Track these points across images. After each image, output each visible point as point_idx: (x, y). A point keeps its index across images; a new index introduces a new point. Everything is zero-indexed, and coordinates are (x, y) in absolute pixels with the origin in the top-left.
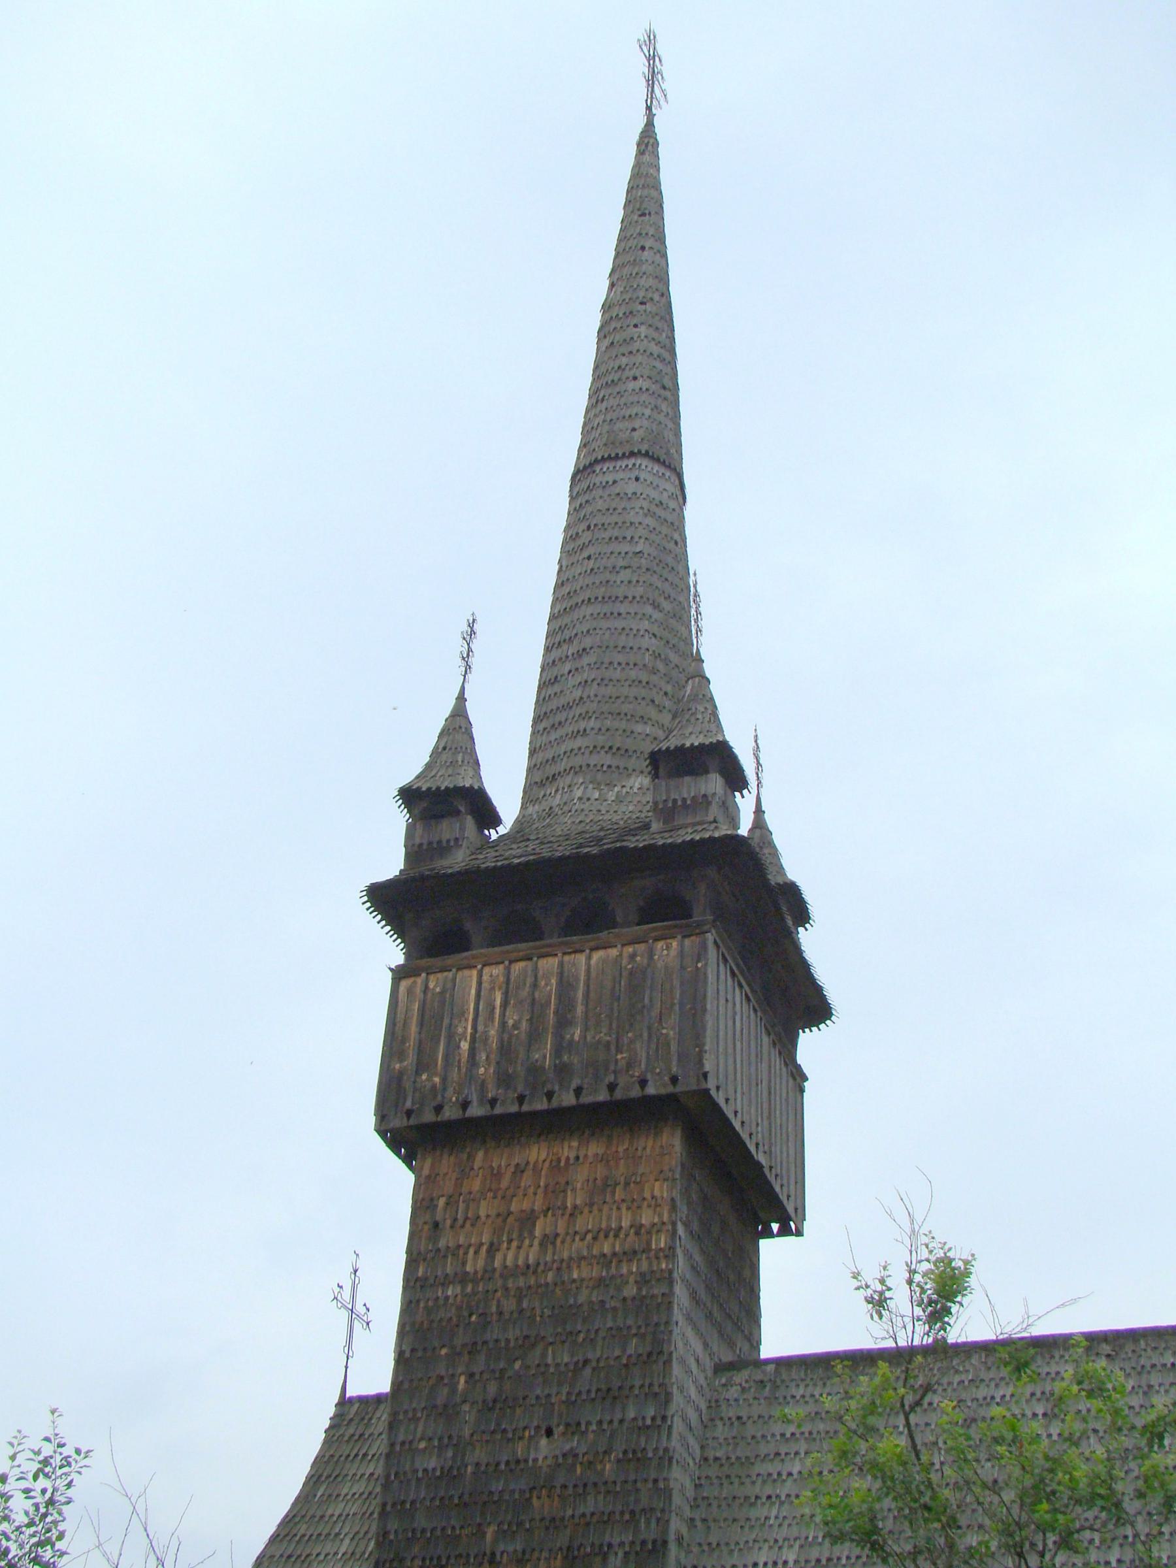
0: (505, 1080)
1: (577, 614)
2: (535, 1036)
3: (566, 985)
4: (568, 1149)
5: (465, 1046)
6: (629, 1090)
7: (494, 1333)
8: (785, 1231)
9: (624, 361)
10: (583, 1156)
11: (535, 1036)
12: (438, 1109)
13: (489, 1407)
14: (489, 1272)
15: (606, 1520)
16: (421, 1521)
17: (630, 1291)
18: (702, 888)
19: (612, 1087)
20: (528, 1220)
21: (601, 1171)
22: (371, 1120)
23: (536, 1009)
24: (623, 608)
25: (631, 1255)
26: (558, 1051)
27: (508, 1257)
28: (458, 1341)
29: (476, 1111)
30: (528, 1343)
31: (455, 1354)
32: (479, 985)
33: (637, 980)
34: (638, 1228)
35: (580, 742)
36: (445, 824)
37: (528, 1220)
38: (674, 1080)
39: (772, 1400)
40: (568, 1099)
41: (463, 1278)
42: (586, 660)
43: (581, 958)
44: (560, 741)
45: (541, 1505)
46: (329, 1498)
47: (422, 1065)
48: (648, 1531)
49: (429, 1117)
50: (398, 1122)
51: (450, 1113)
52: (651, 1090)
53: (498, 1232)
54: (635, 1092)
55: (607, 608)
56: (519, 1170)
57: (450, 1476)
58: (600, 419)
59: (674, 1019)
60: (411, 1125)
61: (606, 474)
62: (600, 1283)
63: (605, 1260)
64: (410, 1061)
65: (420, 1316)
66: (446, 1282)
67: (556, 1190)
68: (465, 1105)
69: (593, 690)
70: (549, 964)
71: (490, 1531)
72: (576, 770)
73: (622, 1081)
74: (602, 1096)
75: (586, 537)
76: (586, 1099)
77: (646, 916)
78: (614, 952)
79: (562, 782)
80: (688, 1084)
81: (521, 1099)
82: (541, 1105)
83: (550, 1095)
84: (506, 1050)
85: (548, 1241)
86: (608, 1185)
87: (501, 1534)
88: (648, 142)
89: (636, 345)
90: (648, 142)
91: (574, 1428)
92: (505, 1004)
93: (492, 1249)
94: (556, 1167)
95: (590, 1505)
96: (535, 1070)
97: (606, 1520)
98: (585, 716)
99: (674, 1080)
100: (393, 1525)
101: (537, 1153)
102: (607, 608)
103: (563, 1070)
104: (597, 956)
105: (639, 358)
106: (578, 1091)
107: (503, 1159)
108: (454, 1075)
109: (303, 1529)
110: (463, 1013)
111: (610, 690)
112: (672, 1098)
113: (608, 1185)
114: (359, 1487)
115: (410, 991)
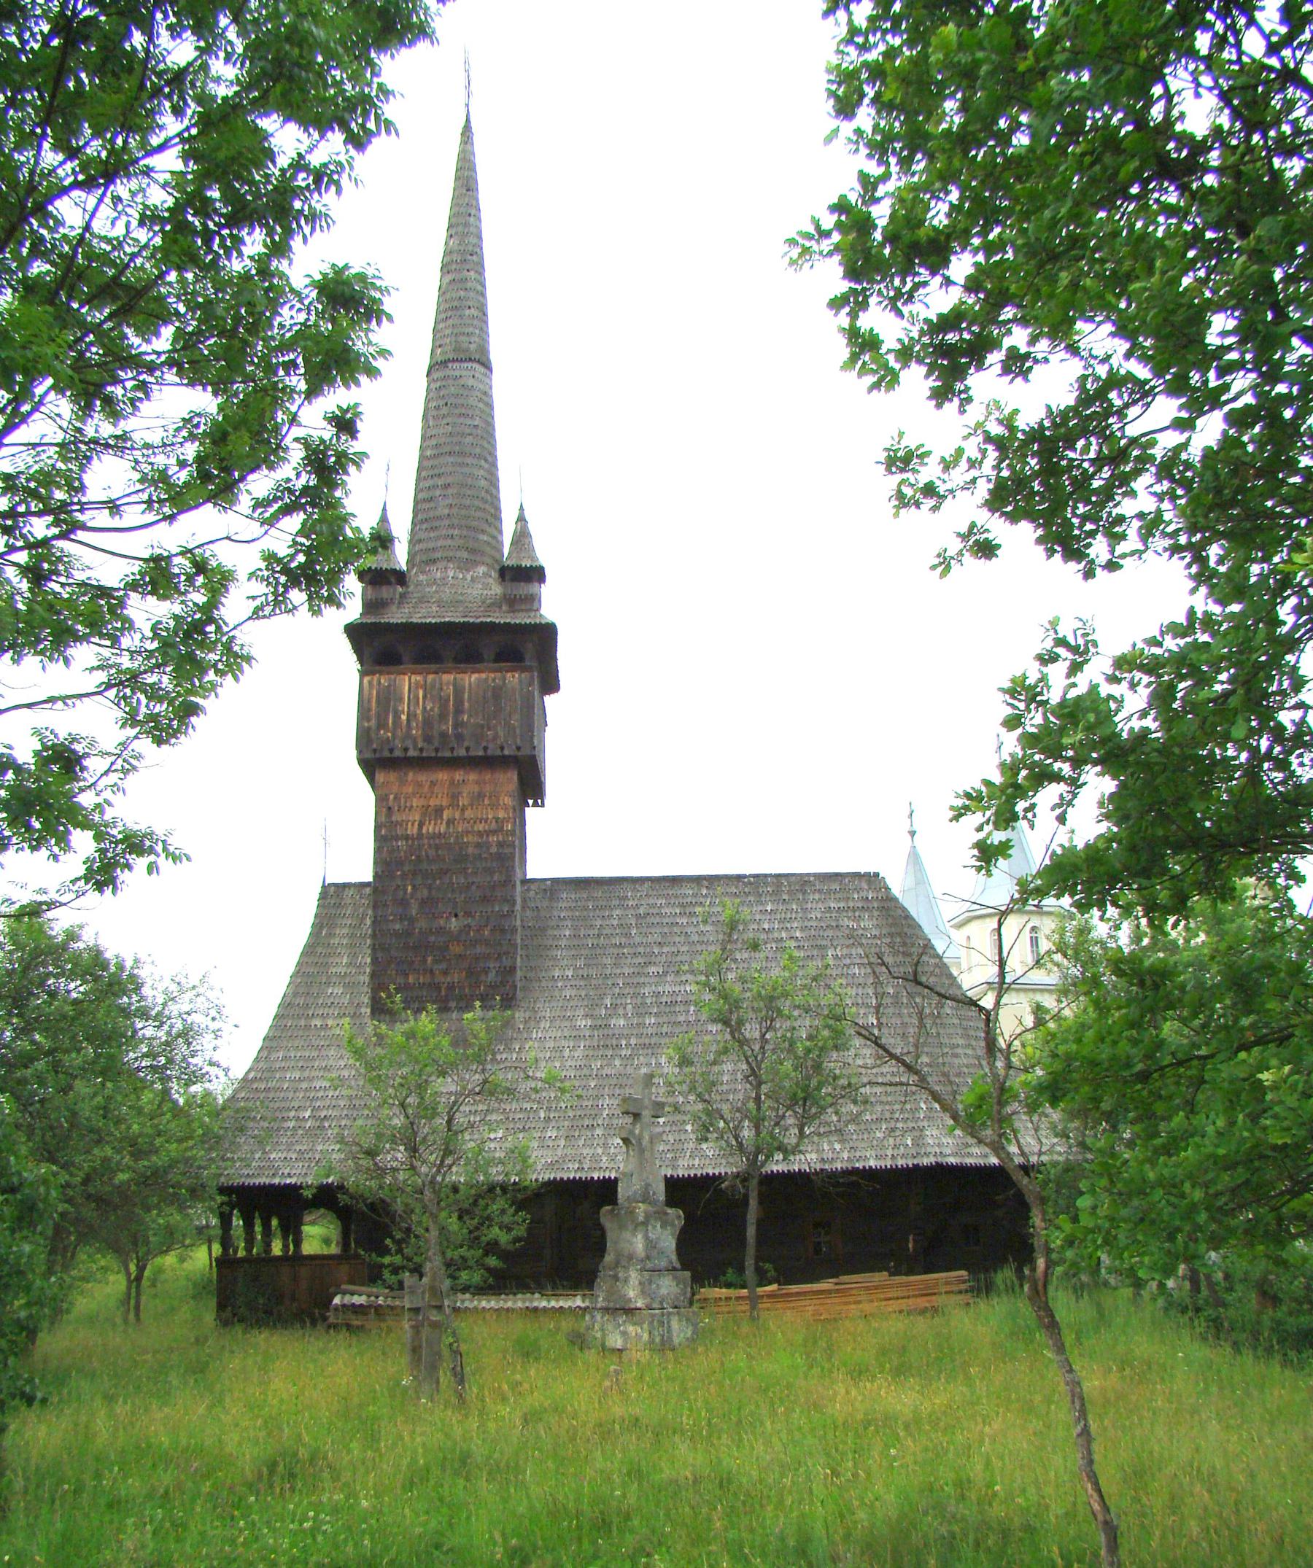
0: (428, 739)
1: (441, 460)
2: (443, 716)
3: (458, 692)
4: (459, 775)
5: (404, 717)
6: (493, 751)
7: (424, 866)
8: (535, 805)
9: (462, 293)
10: (470, 780)
11: (443, 716)
12: (391, 751)
13: (423, 902)
14: (420, 836)
15: (487, 957)
16: (394, 953)
17: (494, 850)
18: (530, 645)
19: (485, 749)
20: (439, 811)
21: (476, 789)
22: (353, 753)
23: (444, 702)
24: (469, 460)
25: (494, 832)
26: (456, 726)
27: (429, 828)
28: (406, 868)
29: (411, 753)
30: (443, 872)
31: (404, 876)
32: (407, 683)
33: (497, 693)
34: (497, 819)
35: (449, 542)
36: (384, 588)
37: (439, 811)
38: (519, 748)
39: (551, 899)
40: (462, 753)
41: (407, 838)
42: (450, 491)
43: (466, 677)
44: (437, 538)
45: (456, 949)
46: (330, 935)
47: (382, 725)
48: (507, 962)
49: (386, 754)
50: (369, 755)
51: (398, 753)
52: (506, 752)
53: (424, 815)
54: (498, 753)
55: (460, 460)
56: (433, 784)
57: (408, 933)
58: (448, 332)
59: (517, 716)
60: (377, 759)
61: (455, 369)
62: (478, 845)
63: (480, 834)
64: (373, 723)
65: (385, 854)
66: (397, 838)
67: (454, 797)
68: (406, 750)
69: (455, 511)
70: (446, 677)
71: (430, 959)
72: (449, 559)
73: (491, 746)
74: (481, 753)
75: (445, 411)
76: (472, 753)
77: (500, 658)
78: (484, 676)
79: (441, 565)
80: (526, 751)
81: (437, 750)
82: (448, 754)
83: (452, 749)
84: (427, 723)
85: (450, 822)
86: (480, 796)
87: (436, 961)
88: (467, 130)
89: (469, 285)
90: (467, 130)
91: (468, 914)
92: (425, 697)
93: (421, 825)
94: (452, 782)
95: (478, 950)
96: (444, 735)
97: (487, 957)
98: (452, 526)
99: (519, 748)
100: (380, 955)
101: (442, 776)
102: (460, 460)
103: (459, 737)
104: (474, 677)
105: (472, 294)
106: (468, 749)
107: (423, 777)
108: (399, 733)
109: (319, 950)
110: (401, 699)
111: (463, 512)
112: (515, 757)
113: (480, 796)
114: (345, 931)
115: (370, 683)
